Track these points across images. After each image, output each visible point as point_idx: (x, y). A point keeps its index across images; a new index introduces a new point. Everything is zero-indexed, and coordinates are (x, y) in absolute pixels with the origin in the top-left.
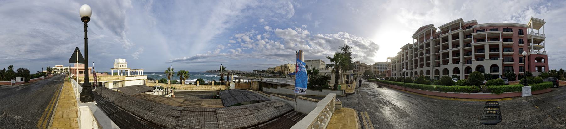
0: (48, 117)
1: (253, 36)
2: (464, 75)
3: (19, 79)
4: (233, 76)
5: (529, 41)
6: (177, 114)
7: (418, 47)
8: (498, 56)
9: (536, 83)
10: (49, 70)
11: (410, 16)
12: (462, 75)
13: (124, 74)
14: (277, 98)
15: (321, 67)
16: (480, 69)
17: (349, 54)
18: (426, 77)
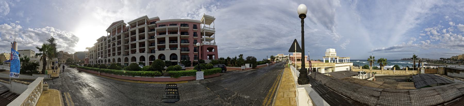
0: (271, 96)
1: (440, 30)
2: (148, 62)
3: (247, 66)
4: (423, 63)
5: (202, 34)
6: (377, 94)
7: (111, 39)
8: (176, 46)
9: (207, 69)
10: (273, 58)
11: (104, 14)
12: (147, 62)
13: (334, 61)
14: (459, 81)
15: (31, 56)
16: (162, 58)
17: (55, 45)
18: (118, 64)
